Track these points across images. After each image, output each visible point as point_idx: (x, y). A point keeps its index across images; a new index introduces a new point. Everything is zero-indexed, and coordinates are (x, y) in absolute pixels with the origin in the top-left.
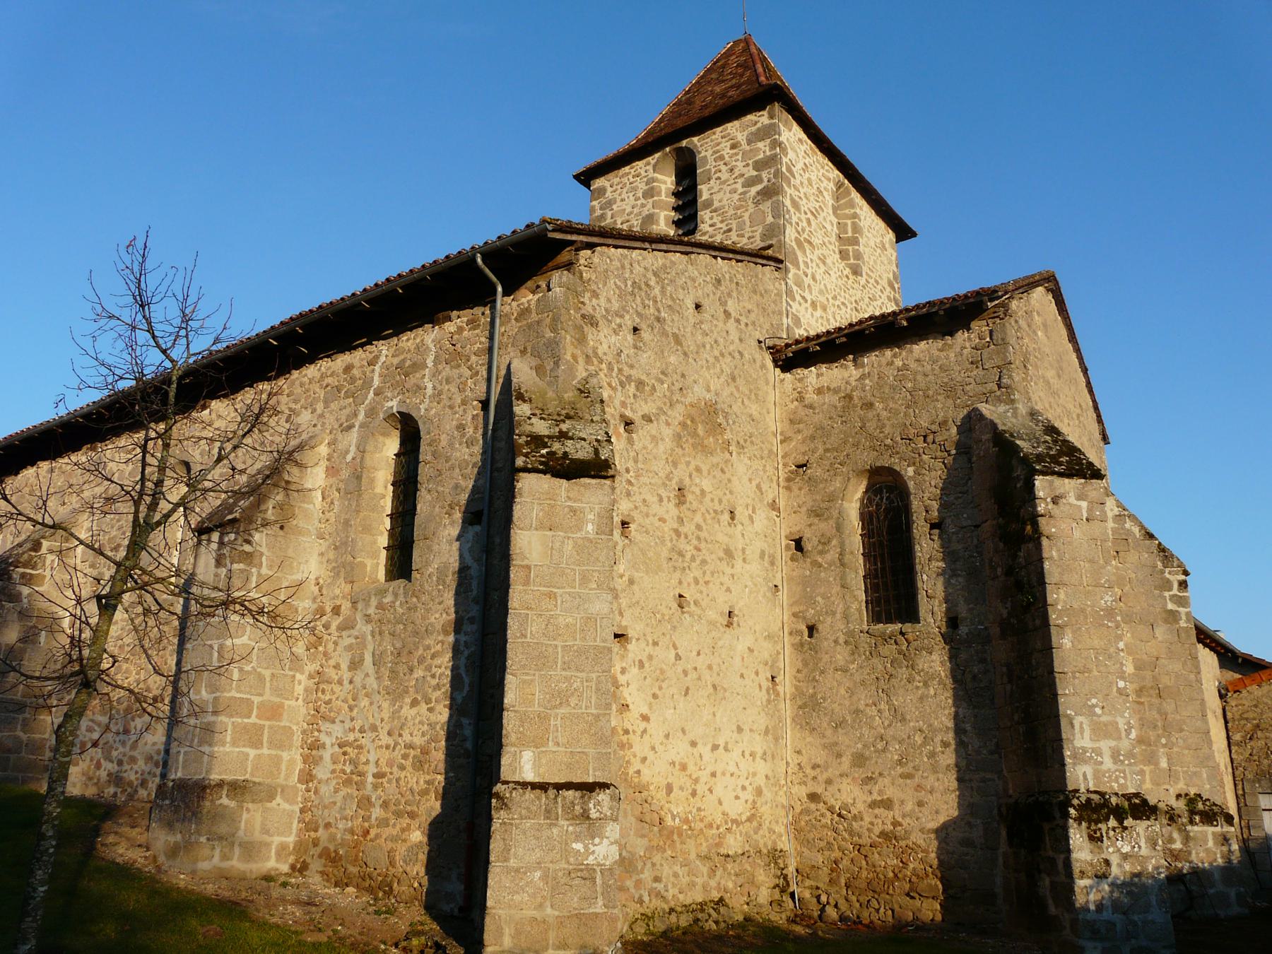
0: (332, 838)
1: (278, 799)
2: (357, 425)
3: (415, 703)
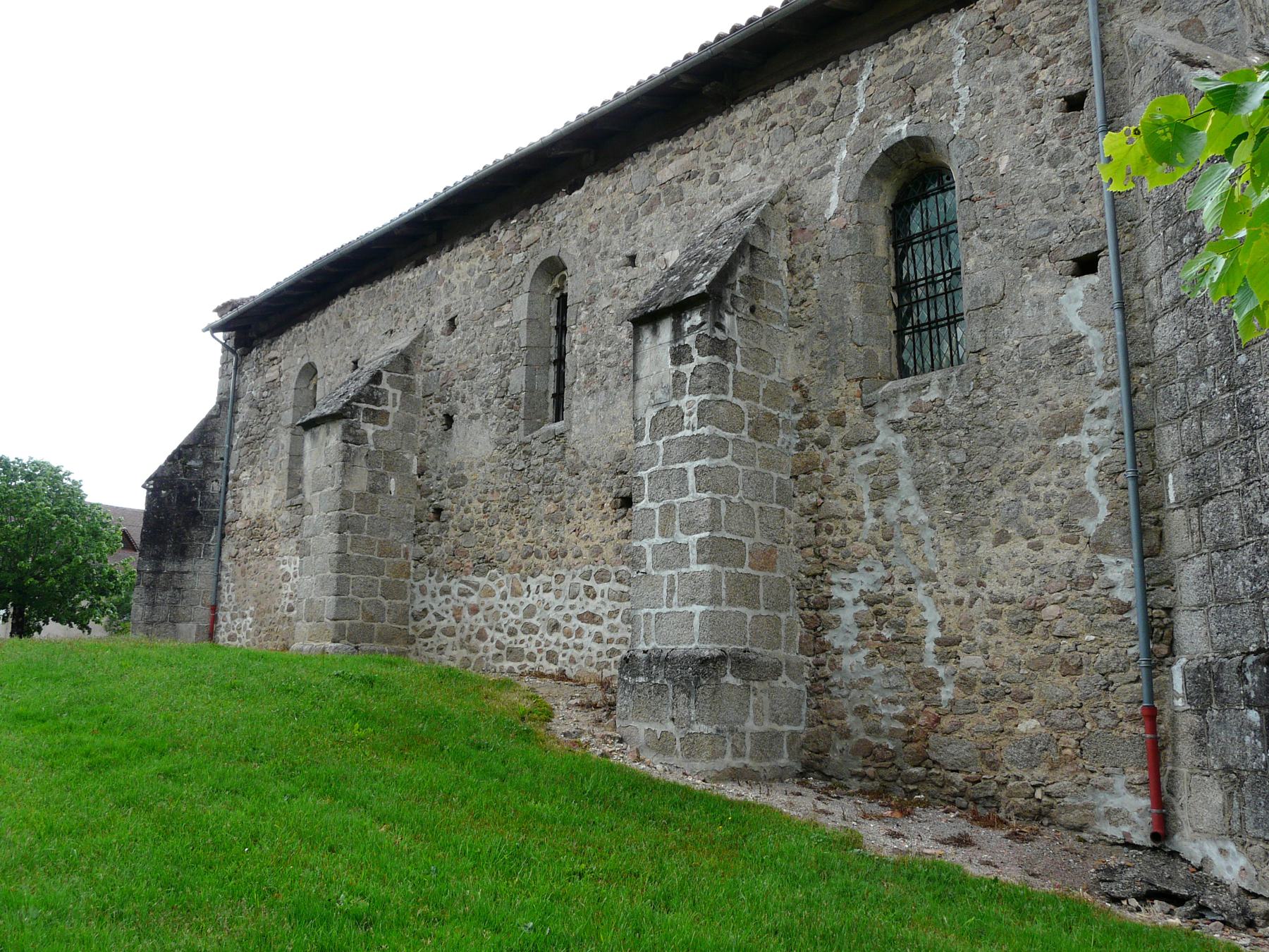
0: (875, 731)
1: (784, 677)
2: (837, 167)
3: (1002, 538)
